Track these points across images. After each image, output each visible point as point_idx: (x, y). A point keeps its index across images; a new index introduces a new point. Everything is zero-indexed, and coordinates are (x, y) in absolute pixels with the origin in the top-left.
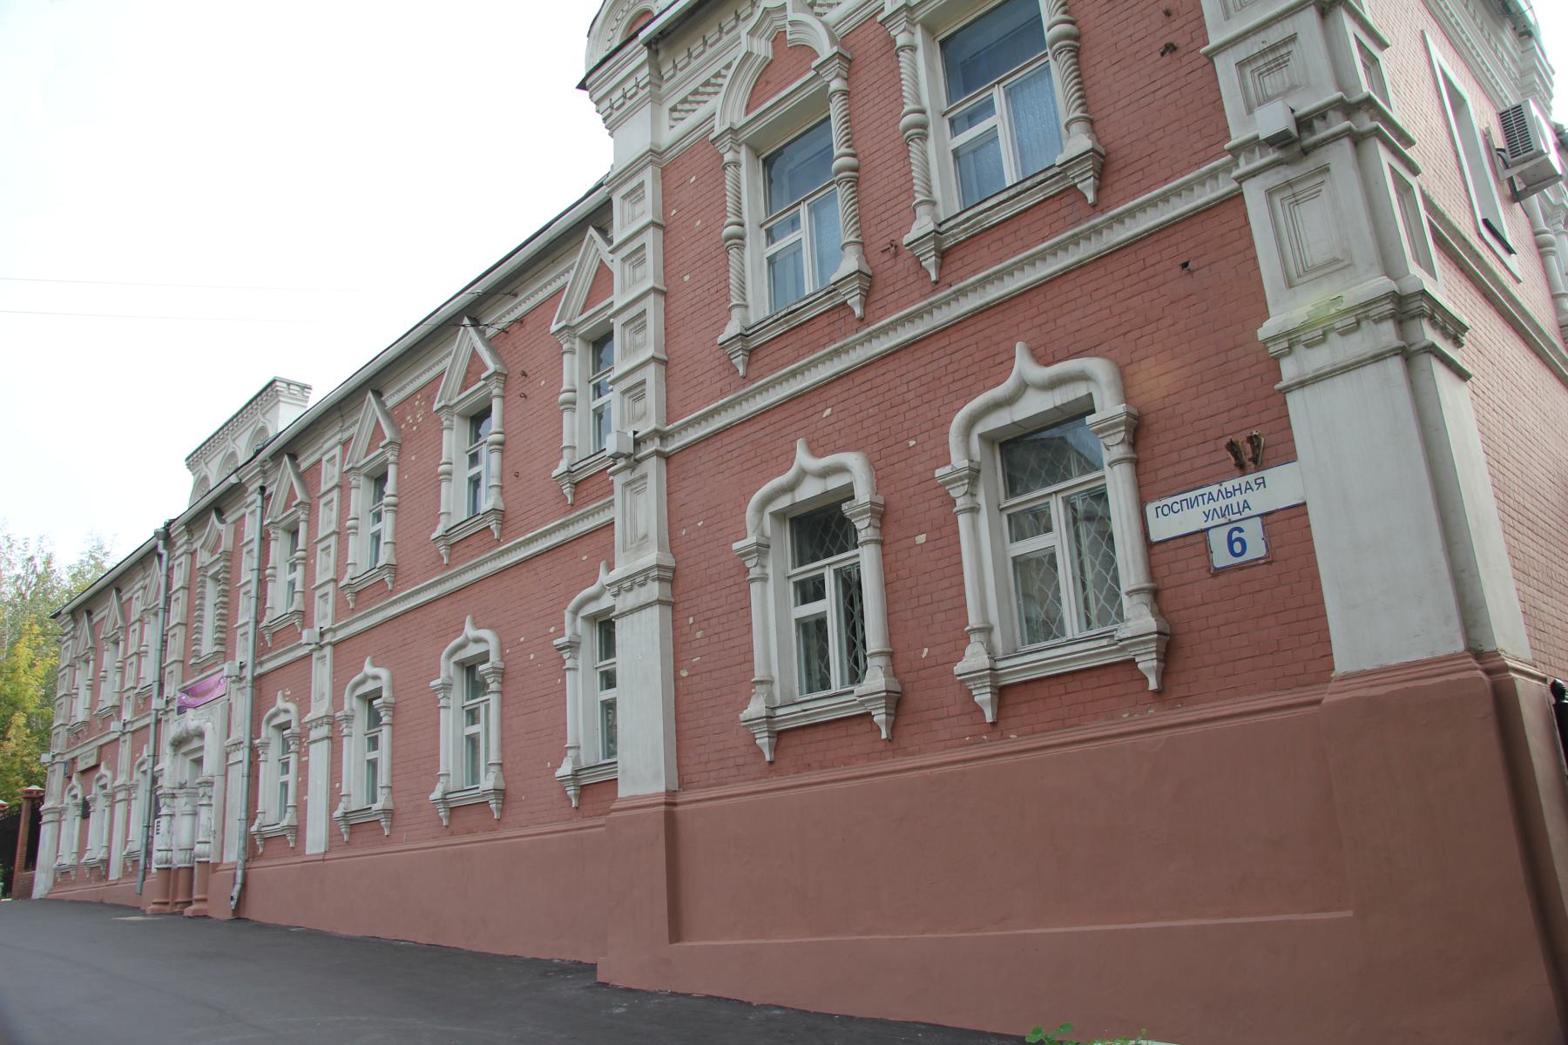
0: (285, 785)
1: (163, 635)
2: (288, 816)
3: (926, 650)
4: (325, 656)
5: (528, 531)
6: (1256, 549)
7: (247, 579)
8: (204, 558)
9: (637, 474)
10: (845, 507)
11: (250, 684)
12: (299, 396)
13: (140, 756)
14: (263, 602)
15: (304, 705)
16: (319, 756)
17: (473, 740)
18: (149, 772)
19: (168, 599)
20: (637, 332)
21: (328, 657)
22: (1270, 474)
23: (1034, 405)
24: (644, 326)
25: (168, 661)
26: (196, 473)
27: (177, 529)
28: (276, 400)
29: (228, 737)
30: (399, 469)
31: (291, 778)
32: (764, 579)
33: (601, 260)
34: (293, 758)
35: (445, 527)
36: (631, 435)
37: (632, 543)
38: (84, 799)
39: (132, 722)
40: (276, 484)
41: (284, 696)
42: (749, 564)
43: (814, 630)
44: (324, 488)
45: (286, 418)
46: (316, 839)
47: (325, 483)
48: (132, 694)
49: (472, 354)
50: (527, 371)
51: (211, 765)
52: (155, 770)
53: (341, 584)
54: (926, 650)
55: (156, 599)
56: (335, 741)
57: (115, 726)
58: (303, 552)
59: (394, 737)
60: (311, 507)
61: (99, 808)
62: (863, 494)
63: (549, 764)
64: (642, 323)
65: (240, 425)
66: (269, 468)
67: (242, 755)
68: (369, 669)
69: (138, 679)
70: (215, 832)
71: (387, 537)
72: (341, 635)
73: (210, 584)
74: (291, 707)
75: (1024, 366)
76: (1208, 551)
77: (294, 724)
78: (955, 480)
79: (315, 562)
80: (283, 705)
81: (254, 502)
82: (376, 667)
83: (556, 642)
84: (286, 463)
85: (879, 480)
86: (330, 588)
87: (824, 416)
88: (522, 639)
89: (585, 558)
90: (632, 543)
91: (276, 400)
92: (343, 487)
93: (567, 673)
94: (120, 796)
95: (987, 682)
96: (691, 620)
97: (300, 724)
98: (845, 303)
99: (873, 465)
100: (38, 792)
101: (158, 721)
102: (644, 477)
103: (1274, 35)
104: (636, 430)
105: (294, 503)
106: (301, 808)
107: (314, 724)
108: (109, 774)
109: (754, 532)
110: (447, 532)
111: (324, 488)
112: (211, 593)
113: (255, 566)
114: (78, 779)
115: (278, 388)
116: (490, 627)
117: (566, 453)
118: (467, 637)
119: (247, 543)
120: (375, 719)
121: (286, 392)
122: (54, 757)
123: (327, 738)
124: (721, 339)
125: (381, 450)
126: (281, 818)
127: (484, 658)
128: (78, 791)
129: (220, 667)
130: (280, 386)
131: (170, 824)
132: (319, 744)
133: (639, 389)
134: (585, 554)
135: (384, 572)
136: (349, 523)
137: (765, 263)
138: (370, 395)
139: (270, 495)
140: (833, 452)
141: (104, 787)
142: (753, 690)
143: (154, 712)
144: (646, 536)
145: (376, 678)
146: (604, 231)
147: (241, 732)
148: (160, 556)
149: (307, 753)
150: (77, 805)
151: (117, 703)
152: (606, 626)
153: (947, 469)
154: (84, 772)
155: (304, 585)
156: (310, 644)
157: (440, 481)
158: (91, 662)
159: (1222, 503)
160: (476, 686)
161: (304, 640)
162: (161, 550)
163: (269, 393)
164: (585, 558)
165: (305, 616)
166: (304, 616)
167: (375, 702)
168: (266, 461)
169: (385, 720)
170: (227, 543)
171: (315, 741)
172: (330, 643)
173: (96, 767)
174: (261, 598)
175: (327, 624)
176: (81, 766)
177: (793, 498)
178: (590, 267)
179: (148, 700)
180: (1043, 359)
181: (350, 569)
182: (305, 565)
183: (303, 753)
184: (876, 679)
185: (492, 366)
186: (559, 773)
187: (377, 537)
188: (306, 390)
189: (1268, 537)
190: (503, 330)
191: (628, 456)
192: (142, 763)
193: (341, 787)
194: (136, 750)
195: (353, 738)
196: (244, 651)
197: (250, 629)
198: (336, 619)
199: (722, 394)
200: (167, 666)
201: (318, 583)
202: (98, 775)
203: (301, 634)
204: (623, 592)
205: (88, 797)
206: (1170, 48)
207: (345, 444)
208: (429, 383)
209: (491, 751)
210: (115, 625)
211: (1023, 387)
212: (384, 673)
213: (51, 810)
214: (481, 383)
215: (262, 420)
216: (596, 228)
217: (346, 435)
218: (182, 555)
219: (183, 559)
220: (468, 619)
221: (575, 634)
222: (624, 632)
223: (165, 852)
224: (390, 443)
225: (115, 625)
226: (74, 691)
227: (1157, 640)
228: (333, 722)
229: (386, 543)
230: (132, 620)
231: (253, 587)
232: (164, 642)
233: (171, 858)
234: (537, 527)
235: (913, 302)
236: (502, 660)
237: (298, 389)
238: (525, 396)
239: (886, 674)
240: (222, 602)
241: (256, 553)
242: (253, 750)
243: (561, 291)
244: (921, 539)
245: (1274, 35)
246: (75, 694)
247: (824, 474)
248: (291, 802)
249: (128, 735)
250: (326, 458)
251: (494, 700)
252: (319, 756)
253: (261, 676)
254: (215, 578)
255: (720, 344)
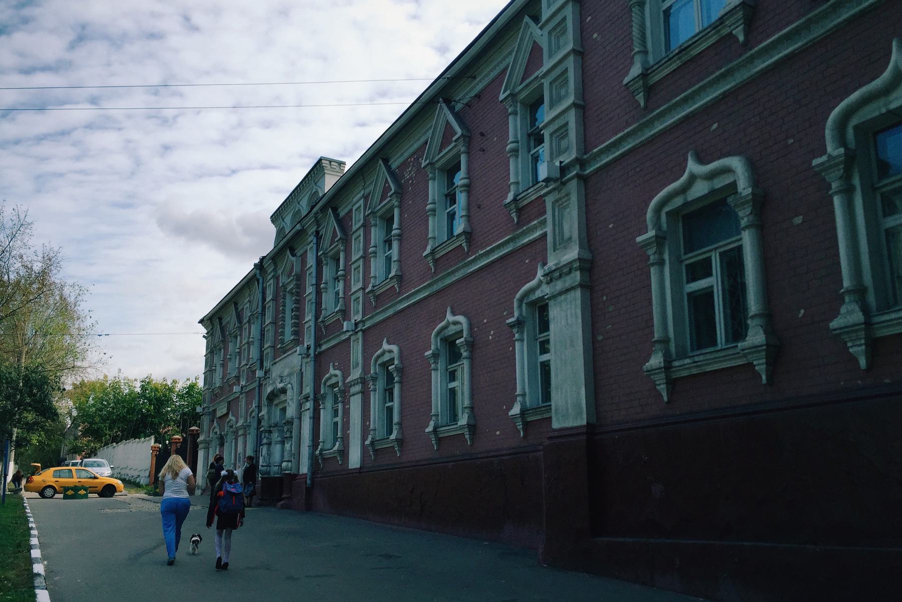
0: (336, 424)
1: (261, 330)
2: (337, 443)
3: (802, 311)
4: (359, 339)
5: (488, 245)
7: (310, 291)
8: (283, 280)
9: (563, 192)
10: (730, 200)
11: (313, 359)
12: (337, 169)
13: (251, 407)
14: (320, 306)
15: (346, 374)
16: (355, 404)
17: (453, 392)
18: (256, 417)
19: (264, 308)
20: (561, 87)
21: (360, 339)
24: (566, 81)
25: (265, 347)
26: (277, 226)
27: (267, 262)
28: (323, 173)
29: (301, 393)
30: (401, 211)
31: (339, 419)
33: (534, 41)
34: (340, 406)
35: (432, 247)
36: (557, 164)
37: (560, 245)
38: (221, 434)
39: (246, 386)
40: (324, 229)
41: (334, 366)
42: (650, 252)
43: (701, 302)
44: (354, 228)
45: (330, 182)
46: (355, 459)
47: (355, 224)
48: (245, 368)
50: (484, 131)
51: (291, 412)
52: (260, 415)
53: (367, 291)
54: (802, 311)
55: (257, 308)
56: (365, 395)
57: (236, 389)
58: (343, 272)
59: (402, 390)
60: (346, 240)
61: (229, 438)
62: (744, 187)
63: (505, 407)
64: (565, 80)
65: (308, 185)
66: (320, 218)
67: (309, 405)
68: (386, 346)
69: (248, 360)
70: (294, 454)
71: (395, 257)
72: (368, 325)
73: (288, 296)
74: (338, 372)
75: (692, 166)
77: (340, 384)
78: (830, 167)
79: (351, 278)
80: (334, 373)
81: (312, 241)
82: (391, 344)
83: (508, 321)
84: (330, 214)
85: (756, 178)
86: (360, 294)
87: (712, 130)
88: (485, 321)
89: (527, 261)
90: (560, 245)
91: (323, 173)
92: (366, 226)
93: (516, 343)
94: (241, 432)
95: (862, 334)
96: (605, 298)
97: (344, 383)
98: (731, 33)
99: (752, 166)
100: (197, 431)
101: (260, 385)
102: (567, 195)
104: (562, 160)
105: (454, 139)
106: (345, 440)
107: (353, 383)
108: (234, 419)
109: (653, 228)
110: (433, 250)
111: (354, 228)
112: (290, 303)
113: (314, 282)
114: (217, 422)
115: (323, 164)
116: (464, 314)
117: (512, 187)
118: (448, 321)
119: (309, 268)
120: (390, 379)
121: (329, 167)
122: (204, 409)
123: (243, 435)
124: (625, 82)
125: (389, 198)
126: (334, 446)
127: (459, 334)
128: (217, 430)
129: (295, 349)
130: (325, 163)
131: (268, 449)
132: (356, 397)
133: (563, 130)
134: (527, 259)
135: (393, 281)
136: (371, 250)
137: (662, 15)
138: (380, 162)
139: (322, 235)
140: (719, 158)
141: (231, 427)
142: (654, 348)
143: (258, 379)
144: (570, 238)
145: (390, 351)
146: (536, 19)
147: (308, 389)
148: (258, 281)
149: (349, 403)
150: (217, 438)
151: (238, 375)
152: (541, 308)
153: (824, 158)
154: (220, 418)
155: (344, 293)
156: (348, 331)
157: (428, 216)
158: (222, 350)
160: (454, 356)
161: (345, 329)
162: (258, 276)
163: (318, 169)
164: (527, 261)
165: (345, 313)
166: (345, 313)
167: (390, 368)
168: (318, 213)
169: (396, 379)
170: (297, 269)
171: (354, 395)
172: (361, 330)
173: (227, 415)
174: (318, 303)
175: (359, 317)
176: (219, 414)
177: (686, 198)
178: (527, 46)
179: (254, 372)
181: (372, 280)
182: (345, 281)
183: (346, 402)
184: (756, 336)
185: (459, 131)
186: (512, 413)
187: (389, 259)
188: (342, 165)
190: (466, 104)
191: (556, 180)
192: (253, 411)
193: (370, 424)
194: (249, 403)
195: (439, 371)
196: (309, 340)
197: (312, 323)
198: (364, 315)
199: (628, 124)
200: (265, 349)
201: (353, 291)
202: (228, 420)
203: (343, 324)
204: (563, 275)
205: (223, 433)
207: (366, 197)
208: (418, 149)
209: (464, 400)
210: (235, 325)
211: (693, 178)
212: (395, 348)
213: (202, 442)
214: (453, 144)
215: (298, 205)
216: (530, 17)
217: (367, 191)
218: (271, 279)
219: (272, 281)
220: (449, 310)
221: (437, 349)
222: (554, 312)
223: (266, 468)
224: (340, 239)
225: (235, 325)
226: (214, 368)
227: (766, 350)
228: (363, 381)
229: (394, 261)
230: (244, 322)
231: (313, 297)
232: (262, 335)
233: (270, 471)
234: (494, 241)
235: (792, 22)
236: (471, 336)
237: (337, 164)
238: (483, 150)
239: (765, 332)
240: (296, 308)
241: (314, 274)
242: (316, 401)
243: (505, 69)
244: (798, 220)
246: (214, 370)
247: (711, 176)
248: (339, 434)
249: (244, 394)
250: (354, 208)
251: (466, 363)
252: (355, 404)
253: (320, 353)
254: (291, 292)
255: (626, 85)
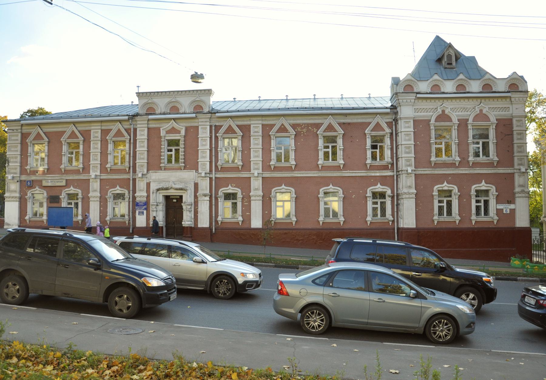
6: (508, 212)
22: (511, 205)
23: (484, 188)
32: (110, 201)
49: (273, 125)
75: (118, 187)
76: (503, 211)
103: (522, 157)
159: (505, 206)
180: (486, 183)
189: (510, 211)
206: (508, 151)
211: (71, 190)
244: (465, 200)
245: (522, 157)
